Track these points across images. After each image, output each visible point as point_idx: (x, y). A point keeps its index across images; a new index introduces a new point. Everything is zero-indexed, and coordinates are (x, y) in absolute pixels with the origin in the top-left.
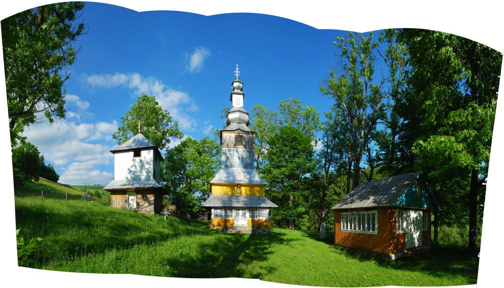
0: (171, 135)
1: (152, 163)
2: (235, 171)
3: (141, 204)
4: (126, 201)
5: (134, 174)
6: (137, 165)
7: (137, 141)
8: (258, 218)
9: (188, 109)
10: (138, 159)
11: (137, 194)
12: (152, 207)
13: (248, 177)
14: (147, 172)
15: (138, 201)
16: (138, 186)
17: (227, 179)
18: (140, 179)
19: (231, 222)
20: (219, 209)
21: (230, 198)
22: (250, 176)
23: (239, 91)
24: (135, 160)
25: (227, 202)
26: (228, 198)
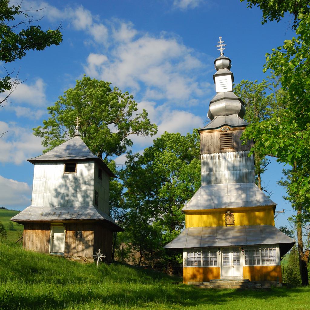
0: (137, 130)
1: (92, 183)
2: (222, 188)
3: (73, 246)
4: (48, 241)
5: (63, 197)
6: (68, 185)
7: (71, 148)
8: (261, 265)
9: (180, 66)
10: (70, 175)
11: (67, 230)
12: (90, 252)
13: (244, 196)
14: (83, 197)
15: (68, 240)
16: (68, 217)
17: (207, 203)
18: (72, 206)
19: (215, 272)
20: (195, 252)
21: (214, 233)
22: (247, 195)
23: (226, 70)
24: (67, 177)
25: (207, 240)
26: (210, 233)
